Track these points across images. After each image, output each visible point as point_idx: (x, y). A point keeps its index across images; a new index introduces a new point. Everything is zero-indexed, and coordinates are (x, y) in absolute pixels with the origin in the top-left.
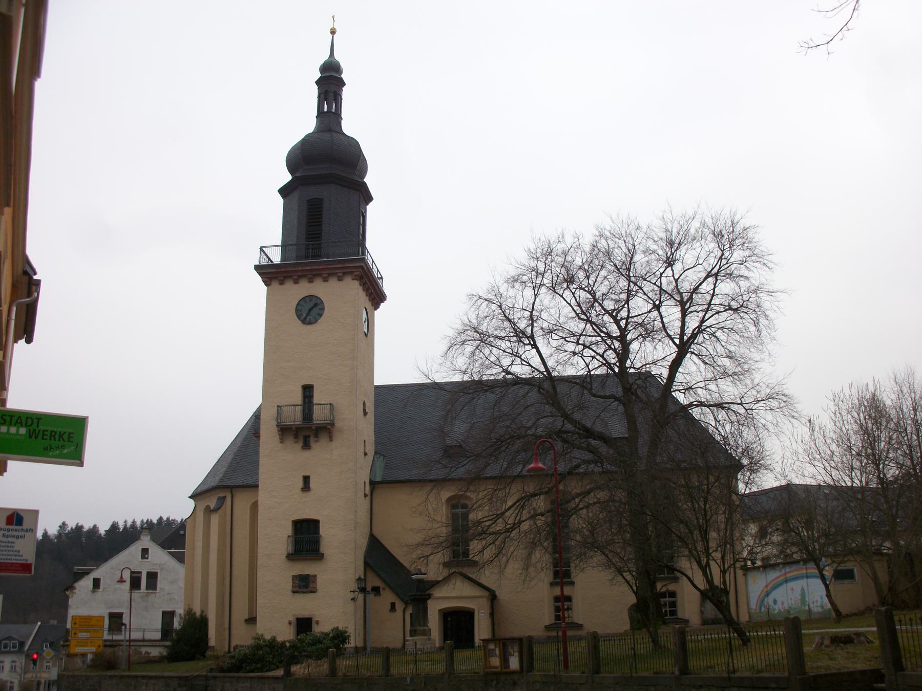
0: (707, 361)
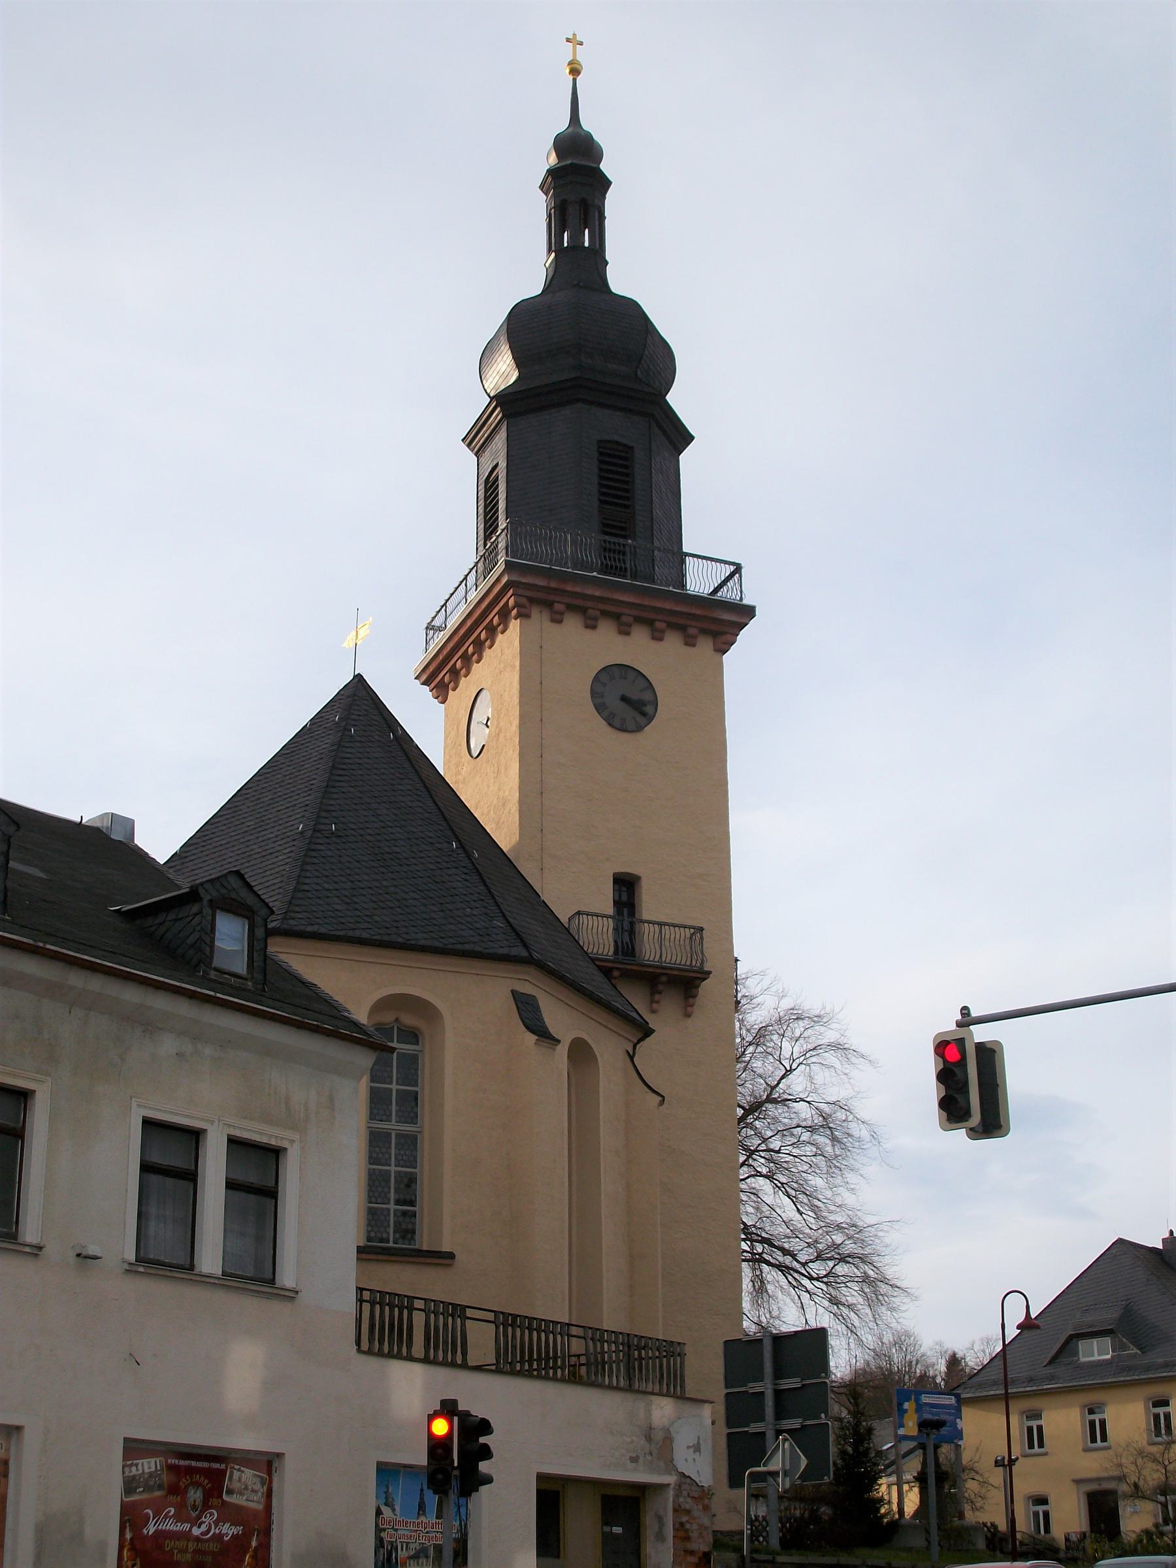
0: (437, 881)
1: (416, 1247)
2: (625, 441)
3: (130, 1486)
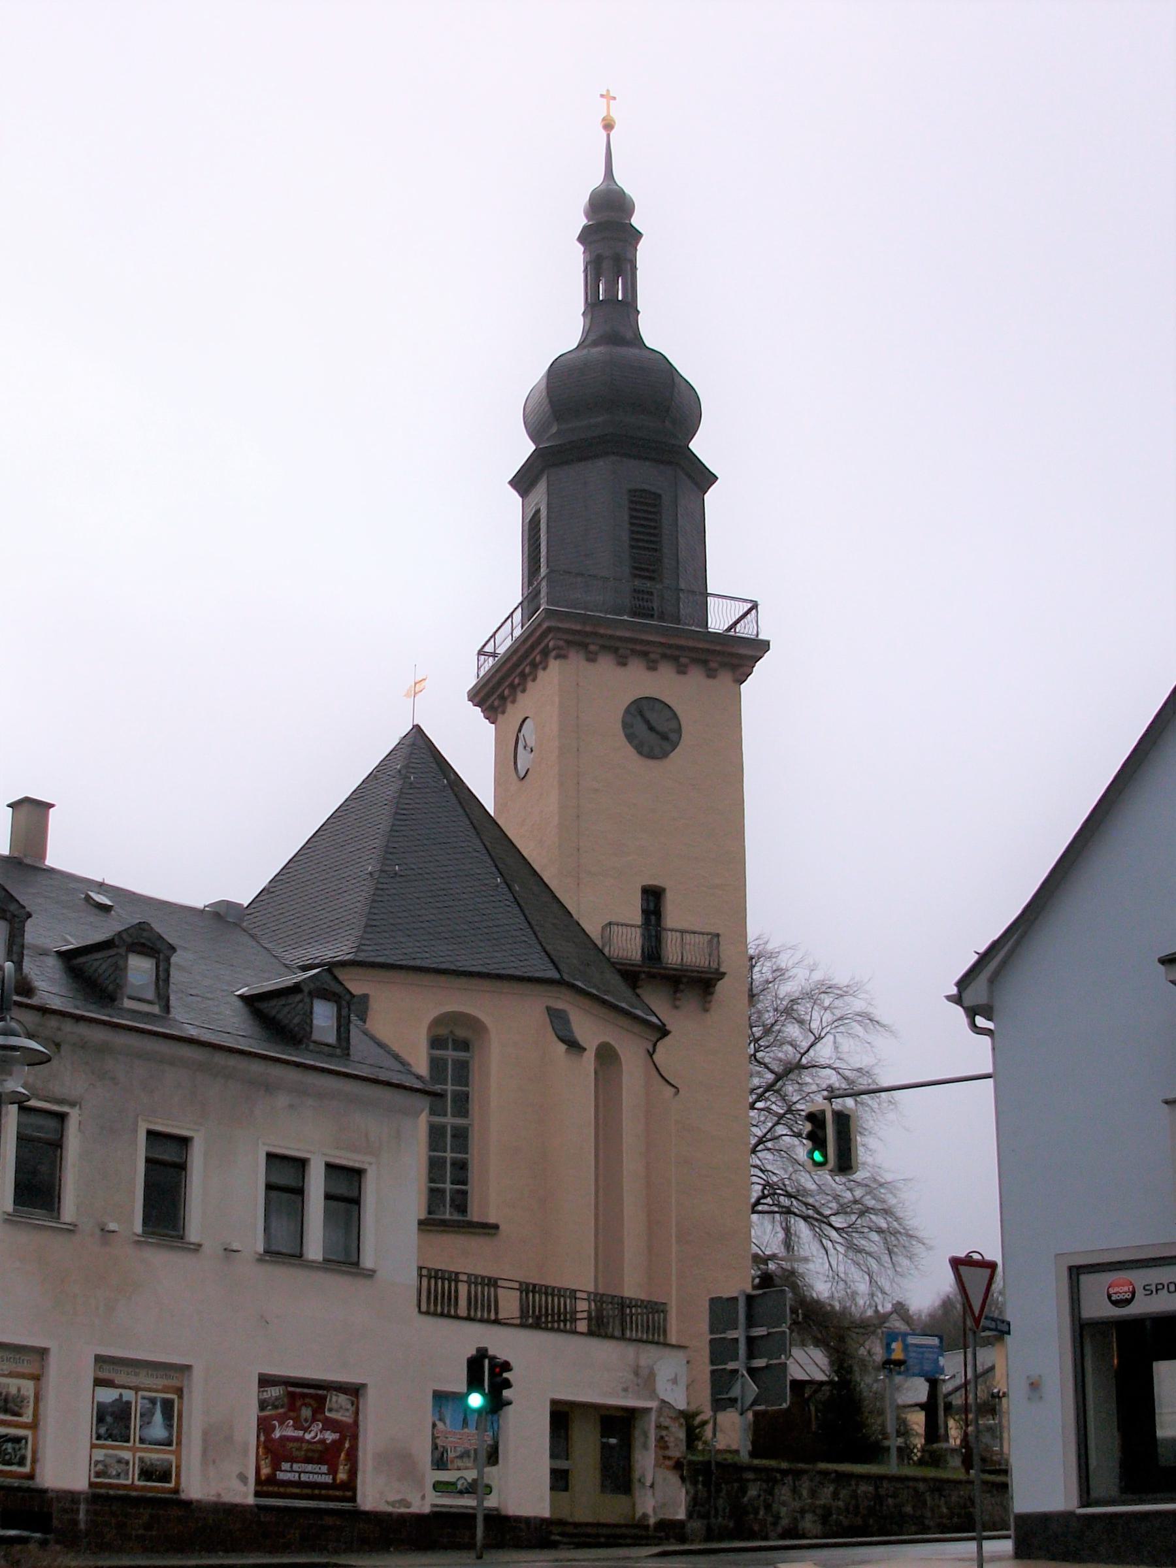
1: (467, 1219)
2: (653, 489)
3: (263, 1405)
